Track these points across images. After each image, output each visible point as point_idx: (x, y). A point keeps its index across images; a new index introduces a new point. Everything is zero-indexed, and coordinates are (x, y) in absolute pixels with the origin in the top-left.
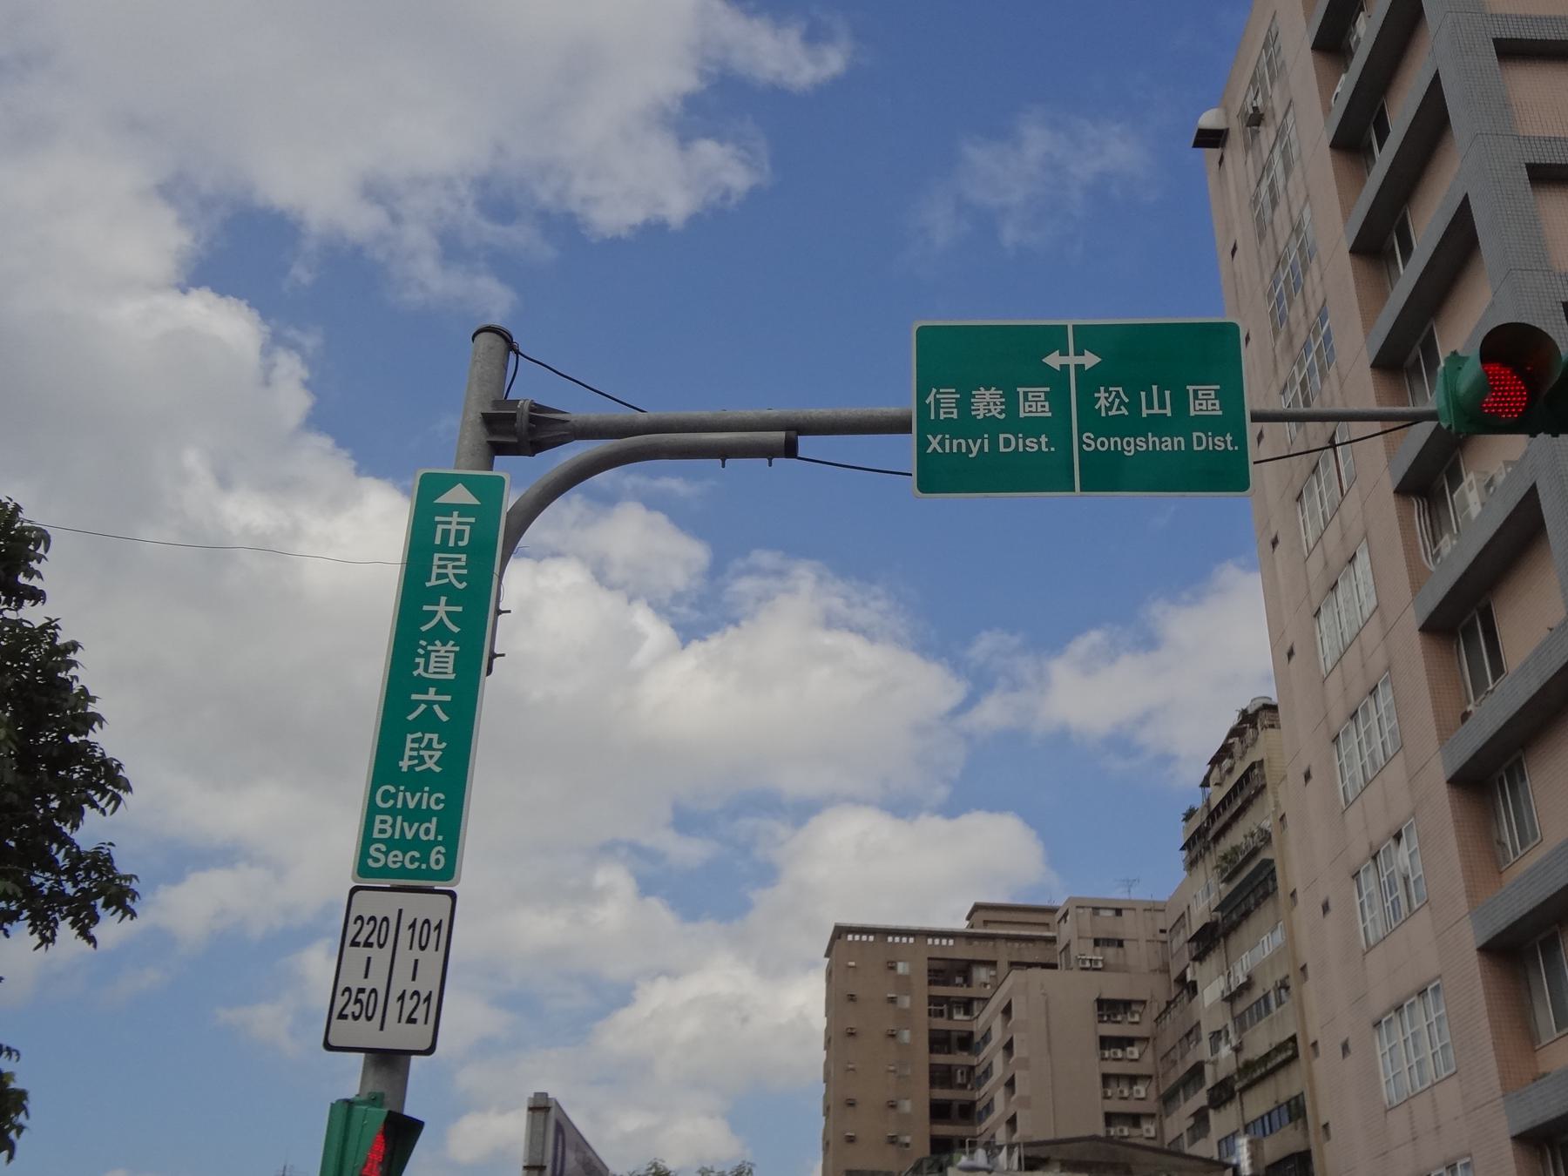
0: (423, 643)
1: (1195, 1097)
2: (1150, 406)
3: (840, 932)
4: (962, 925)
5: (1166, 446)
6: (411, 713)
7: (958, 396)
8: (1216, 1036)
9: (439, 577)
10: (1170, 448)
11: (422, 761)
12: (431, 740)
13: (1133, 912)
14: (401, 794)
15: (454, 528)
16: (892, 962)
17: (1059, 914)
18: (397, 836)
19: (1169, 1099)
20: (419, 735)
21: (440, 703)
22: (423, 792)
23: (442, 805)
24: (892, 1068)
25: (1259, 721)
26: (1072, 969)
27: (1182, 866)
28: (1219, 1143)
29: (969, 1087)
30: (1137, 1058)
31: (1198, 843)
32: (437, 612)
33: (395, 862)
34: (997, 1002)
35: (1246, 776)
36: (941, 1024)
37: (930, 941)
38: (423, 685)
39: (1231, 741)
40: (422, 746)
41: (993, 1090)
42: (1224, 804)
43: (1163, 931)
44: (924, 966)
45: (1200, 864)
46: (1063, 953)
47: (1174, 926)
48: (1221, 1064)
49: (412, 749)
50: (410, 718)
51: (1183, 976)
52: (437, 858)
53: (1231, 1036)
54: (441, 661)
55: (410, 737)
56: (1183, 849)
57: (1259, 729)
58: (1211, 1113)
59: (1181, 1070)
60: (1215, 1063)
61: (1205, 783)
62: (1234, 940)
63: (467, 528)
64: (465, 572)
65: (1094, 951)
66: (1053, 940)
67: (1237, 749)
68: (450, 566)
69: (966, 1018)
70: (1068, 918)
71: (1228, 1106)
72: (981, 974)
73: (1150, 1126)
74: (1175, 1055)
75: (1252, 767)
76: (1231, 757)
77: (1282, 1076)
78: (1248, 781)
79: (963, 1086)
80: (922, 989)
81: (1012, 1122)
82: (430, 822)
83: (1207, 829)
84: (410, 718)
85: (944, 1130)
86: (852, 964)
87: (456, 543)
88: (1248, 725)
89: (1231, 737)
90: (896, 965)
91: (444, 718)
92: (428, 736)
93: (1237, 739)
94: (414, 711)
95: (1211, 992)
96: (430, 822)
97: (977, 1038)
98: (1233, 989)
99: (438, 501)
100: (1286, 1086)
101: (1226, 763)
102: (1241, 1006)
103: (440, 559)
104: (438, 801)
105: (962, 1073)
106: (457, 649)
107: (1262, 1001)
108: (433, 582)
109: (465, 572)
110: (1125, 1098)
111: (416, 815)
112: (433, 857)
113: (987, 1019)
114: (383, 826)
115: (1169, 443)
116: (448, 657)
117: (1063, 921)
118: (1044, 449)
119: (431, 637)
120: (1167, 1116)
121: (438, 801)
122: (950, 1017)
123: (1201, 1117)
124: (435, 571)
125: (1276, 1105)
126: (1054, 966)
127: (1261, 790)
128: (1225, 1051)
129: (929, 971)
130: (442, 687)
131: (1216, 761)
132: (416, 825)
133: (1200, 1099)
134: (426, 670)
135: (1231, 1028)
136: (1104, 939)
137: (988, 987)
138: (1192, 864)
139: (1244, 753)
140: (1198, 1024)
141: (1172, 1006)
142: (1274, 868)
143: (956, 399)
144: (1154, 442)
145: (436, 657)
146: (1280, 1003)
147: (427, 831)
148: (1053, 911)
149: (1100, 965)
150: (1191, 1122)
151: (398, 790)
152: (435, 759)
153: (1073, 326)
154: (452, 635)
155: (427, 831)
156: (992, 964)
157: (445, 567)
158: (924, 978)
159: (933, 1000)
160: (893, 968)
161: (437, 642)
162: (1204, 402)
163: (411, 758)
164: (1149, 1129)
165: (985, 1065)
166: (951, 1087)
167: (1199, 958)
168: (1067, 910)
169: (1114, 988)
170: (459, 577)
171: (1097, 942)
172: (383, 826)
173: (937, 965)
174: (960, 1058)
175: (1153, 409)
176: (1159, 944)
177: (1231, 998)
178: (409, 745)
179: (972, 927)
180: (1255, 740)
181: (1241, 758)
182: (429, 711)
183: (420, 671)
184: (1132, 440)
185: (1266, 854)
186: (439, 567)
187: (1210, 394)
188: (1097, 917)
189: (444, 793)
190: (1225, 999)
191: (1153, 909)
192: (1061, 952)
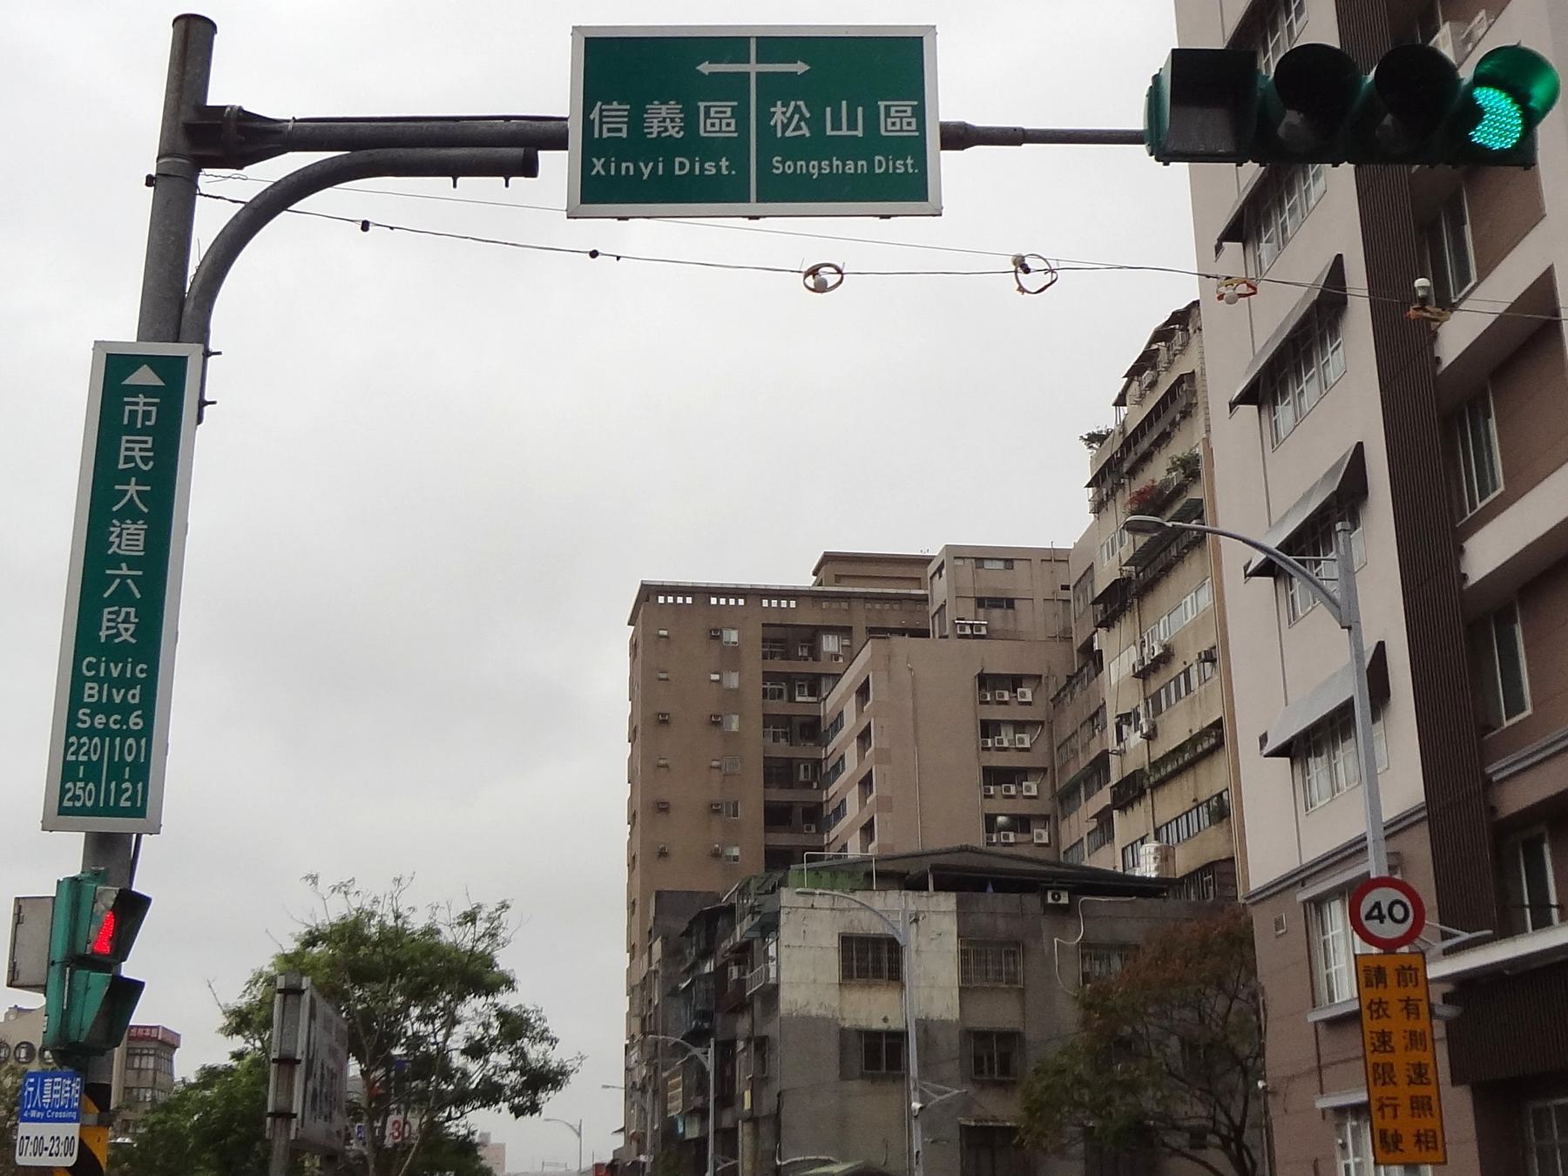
1: (1099, 793)
2: (836, 125)
3: (648, 593)
4: (806, 581)
5: (850, 169)
7: (645, 116)
8: (1125, 719)
9: (128, 459)
10: (852, 171)
12: (128, 614)
13: (1028, 562)
15: (140, 409)
16: (716, 630)
17: (932, 568)
19: (1067, 797)
20: (116, 608)
21: (132, 577)
24: (715, 763)
25: (1190, 320)
26: (946, 637)
27: (1088, 506)
28: (1124, 850)
29: (815, 785)
30: (1014, 748)
31: (1107, 479)
32: (128, 490)
34: (850, 679)
35: (1171, 394)
36: (779, 707)
37: (765, 603)
38: (116, 561)
39: (1155, 347)
40: (120, 620)
41: (844, 788)
42: (1142, 429)
43: (1065, 588)
44: (756, 633)
45: (1110, 504)
46: (937, 616)
47: (1079, 581)
48: (1134, 751)
49: (109, 620)
51: (1090, 642)
52: (135, 722)
53: (1142, 720)
54: (129, 538)
56: (1089, 486)
57: (1191, 331)
58: (1116, 813)
59: (1083, 761)
60: (1121, 753)
61: (1121, 401)
62: (1150, 602)
63: (154, 409)
65: (976, 613)
66: (924, 600)
67: (1163, 357)
68: (137, 450)
69: (810, 699)
70: (944, 572)
71: (1136, 806)
72: (830, 644)
73: (1042, 831)
74: (1077, 743)
75: (1181, 380)
76: (1154, 367)
77: (1202, 769)
78: (1174, 399)
79: (808, 785)
80: (755, 665)
81: (868, 830)
83: (1121, 460)
85: (783, 839)
86: (664, 633)
87: (143, 424)
88: (1177, 326)
89: (1155, 343)
90: (721, 633)
92: (124, 610)
93: (1163, 344)
95: (1120, 664)
97: (826, 724)
98: (1147, 662)
99: (127, 382)
100: (1210, 780)
101: (1147, 376)
102: (1154, 684)
103: (128, 441)
105: (806, 768)
106: (145, 527)
107: (1182, 676)
108: (805, 131)
110: (1012, 797)
111: (125, 683)
112: (132, 720)
113: (839, 699)
114: (91, 692)
115: (852, 167)
116: (139, 535)
117: (937, 575)
118: (725, 172)
119: (123, 515)
120: (1064, 817)
122: (792, 699)
123: (1104, 820)
124: (123, 453)
125: (1195, 804)
126: (924, 633)
127: (1187, 414)
128: (1134, 739)
129: (764, 640)
130: (133, 562)
131: (1134, 373)
132: (123, 691)
133: (1103, 798)
134: (119, 547)
135: (1141, 711)
136: (990, 599)
137: (841, 660)
138: (1099, 507)
139: (1170, 362)
140: (1103, 706)
141: (1074, 681)
142: (1203, 511)
143: (648, 113)
144: (837, 166)
145: (128, 534)
146: (1204, 680)
147: (134, 696)
148: (924, 561)
149: (984, 632)
150: (1094, 824)
152: (130, 633)
153: (749, 62)
154: (141, 515)
156: (845, 631)
157: (132, 449)
158: (758, 650)
159: (768, 676)
160: (718, 638)
162: (898, 120)
163: (108, 628)
164: (1041, 835)
165: (836, 758)
166: (791, 787)
167: (1107, 623)
168: (943, 563)
169: (999, 659)
170: (145, 460)
171: (980, 602)
173: (774, 633)
174: (804, 751)
175: (840, 129)
176: (1061, 603)
177: (1144, 673)
179: (820, 585)
180: (1185, 345)
181: (1167, 369)
182: (123, 584)
183: (114, 548)
184: (816, 163)
185: (1195, 493)
186: (127, 449)
187: (905, 111)
188: (980, 571)
190: (1137, 676)
191: (1054, 558)
192: (933, 617)
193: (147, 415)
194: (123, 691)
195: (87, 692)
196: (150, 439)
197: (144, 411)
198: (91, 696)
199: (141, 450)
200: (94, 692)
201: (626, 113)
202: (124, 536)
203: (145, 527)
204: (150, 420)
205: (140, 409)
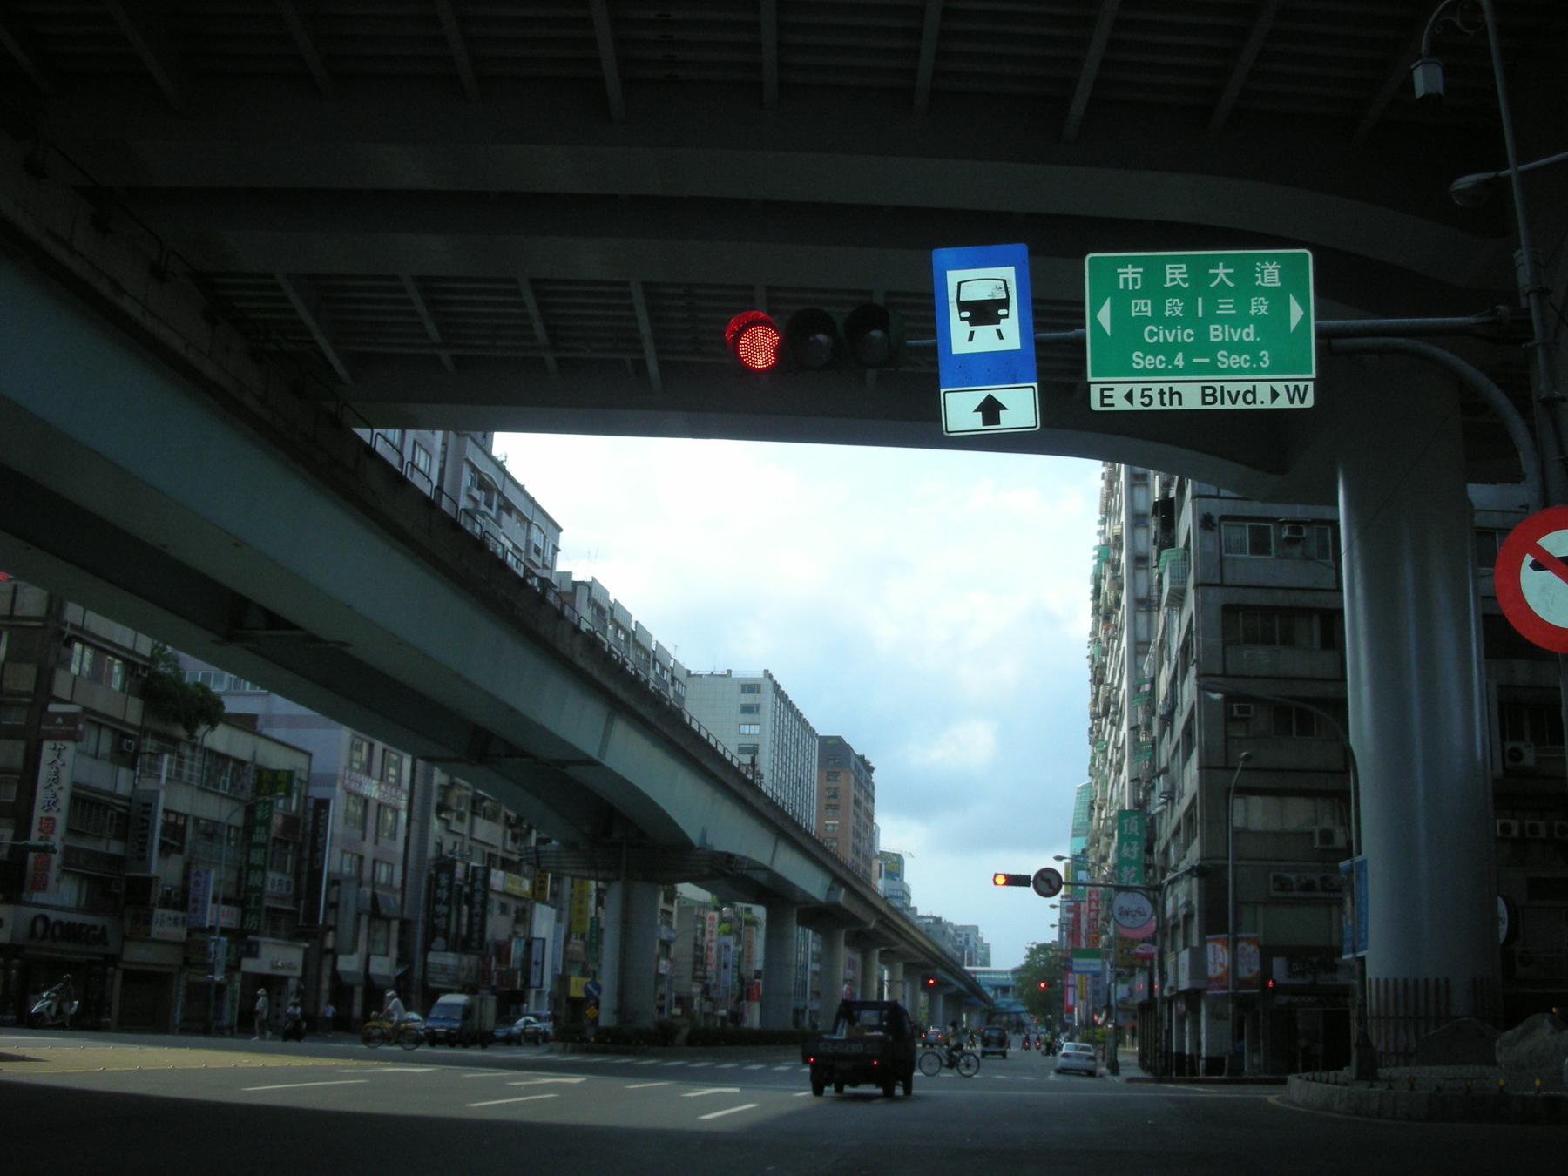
0: (1258, 264)
6: (1213, 282)
9: (1173, 280)
11: (1174, 312)
12: (1176, 302)
14: (1161, 332)
15: (1130, 276)
18: (1227, 339)
22: (1177, 329)
23: (1192, 339)
33: (1235, 364)
50: (1212, 285)
55: (1167, 301)
56: (976, 411)
63: (1139, 276)
64: (1186, 276)
82: (1249, 327)
84: (1212, 285)
87: (1133, 288)
91: (1232, 285)
92: (1175, 300)
94: (1214, 281)
96: (1249, 327)
104: (1189, 336)
106: (1279, 267)
109: (1186, 276)
114: (1216, 333)
121: (1189, 336)
124: (1168, 277)
134: (1263, 281)
147: (1248, 334)
151: (1159, 329)
155: (1248, 334)
157: (1174, 273)
161: (1267, 263)
172: (1216, 333)
178: (1253, 303)
183: (1259, 282)
186: (1171, 274)
189: (1192, 329)
193: (1135, 280)
194: (1239, 330)
195: (1212, 333)
196: (1184, 266)
197: (1133, 278)
198: (1217, 336)
199: (1180, 273)
200: (1219, 333)
201: (1221, 306)
202: (1266, 274)
203: (1279, 267)
204: (1137, 285)
205: (1130, 276)
